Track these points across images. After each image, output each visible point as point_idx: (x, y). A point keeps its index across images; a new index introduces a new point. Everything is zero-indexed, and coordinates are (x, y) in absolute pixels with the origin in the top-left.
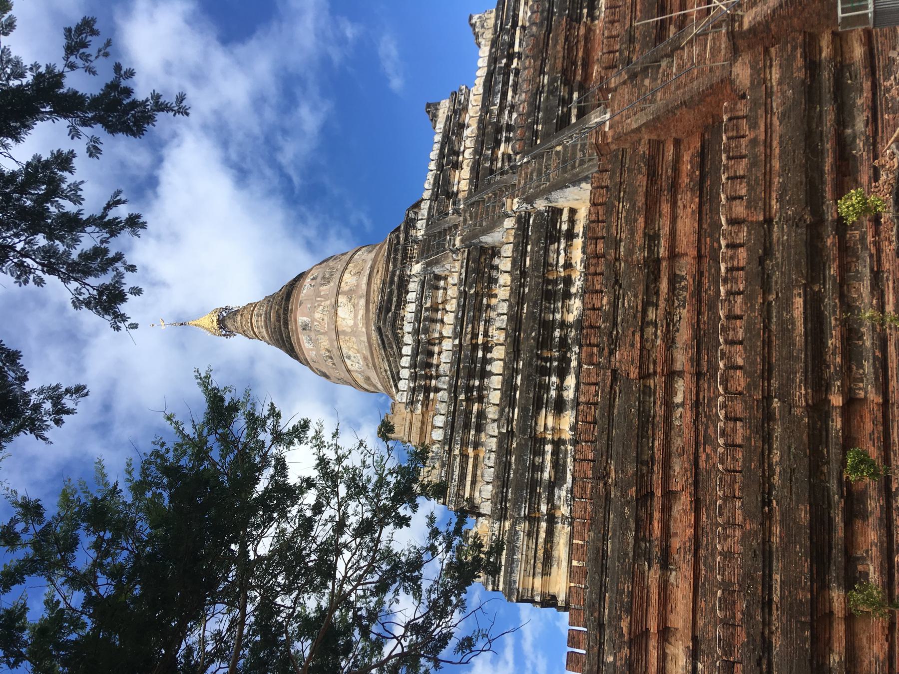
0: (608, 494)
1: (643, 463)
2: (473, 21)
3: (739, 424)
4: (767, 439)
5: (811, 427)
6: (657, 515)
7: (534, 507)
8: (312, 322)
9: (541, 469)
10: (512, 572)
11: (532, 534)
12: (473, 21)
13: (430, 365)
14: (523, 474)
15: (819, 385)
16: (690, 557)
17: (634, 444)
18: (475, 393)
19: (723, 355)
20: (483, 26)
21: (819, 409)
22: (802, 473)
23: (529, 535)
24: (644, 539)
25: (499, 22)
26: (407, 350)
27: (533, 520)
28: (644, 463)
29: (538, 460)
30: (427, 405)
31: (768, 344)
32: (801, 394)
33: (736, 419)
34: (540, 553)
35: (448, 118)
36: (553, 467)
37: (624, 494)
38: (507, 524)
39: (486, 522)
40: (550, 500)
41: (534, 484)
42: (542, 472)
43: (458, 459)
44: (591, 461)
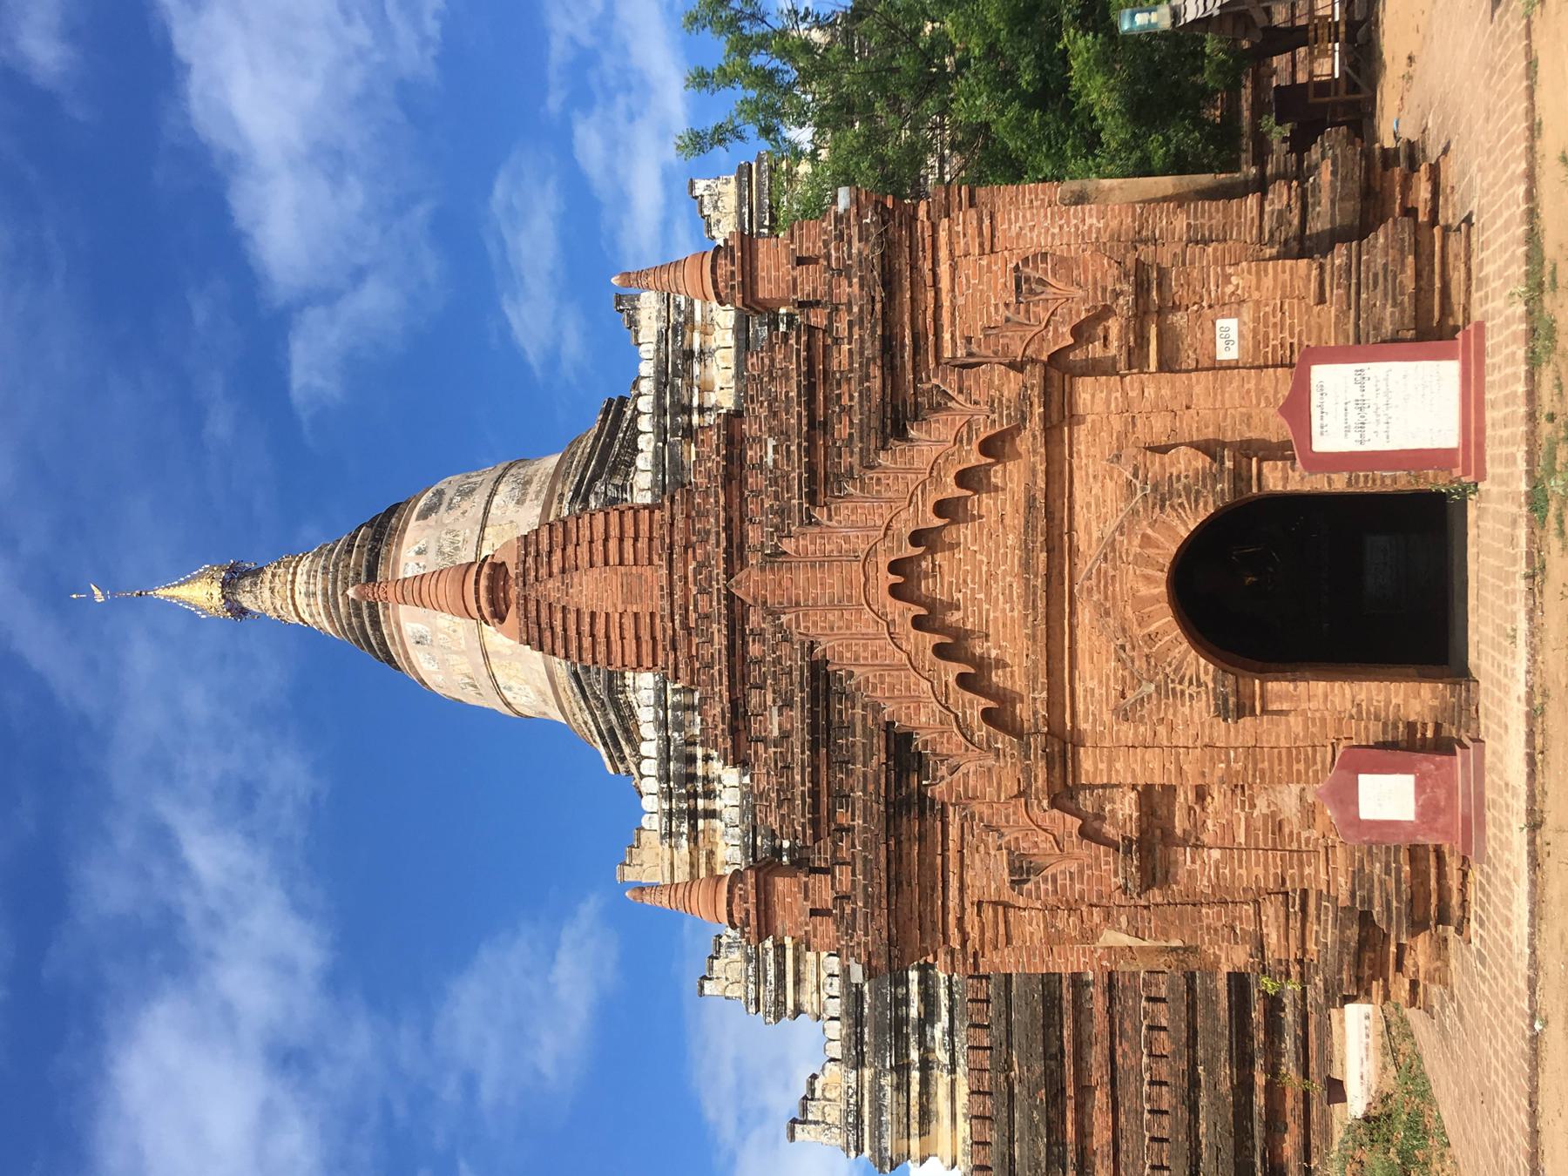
0: (1011, 1088)
1: (1053, 1057)
2: (698, 192)
3: (1164, 1089)
4: (1194, 1109)
5: (1236, 1104)
6: (1070, 1116)
7: (901, 1054)
8: (434, 633)
9: (906, 1001)
10: (881, 1137)
11: (902, 1087)
12: (698, 192)
13: (692, 778)
14: (883, 1014)
15: (1243, 1062)
16: (1109, 1163)
17: (1040, 1037)
18: (785, 859)
19: (1146, 1013)
20: (716, 207)
21: (1244, 1087)
22: (1227, 1154)
23: (897, 1088)
24: (1057, 1144)
25: (746, 210)
26: (649, 749)
27: (902, 1068)
28: (1053, 1057)
29: (901, 991)
30: (696, 838)
31: (1192, 1007)
32: (1225, 1072)
33: (1161, 1083)
34: (915, 1110)
35: (662, 337)
36: (922, 1000)
37: (1031, 1096)
38: (868, 1073)
39: (836, 1069)
40: (922, 1043)
41: (901, 1021)
42: (908, 1006)
43: (771, 954)
44: (985, 1048)
